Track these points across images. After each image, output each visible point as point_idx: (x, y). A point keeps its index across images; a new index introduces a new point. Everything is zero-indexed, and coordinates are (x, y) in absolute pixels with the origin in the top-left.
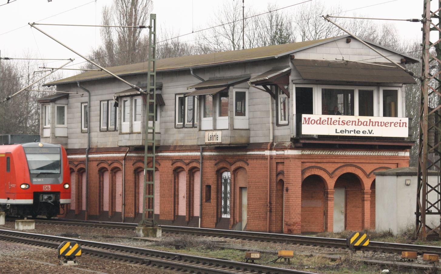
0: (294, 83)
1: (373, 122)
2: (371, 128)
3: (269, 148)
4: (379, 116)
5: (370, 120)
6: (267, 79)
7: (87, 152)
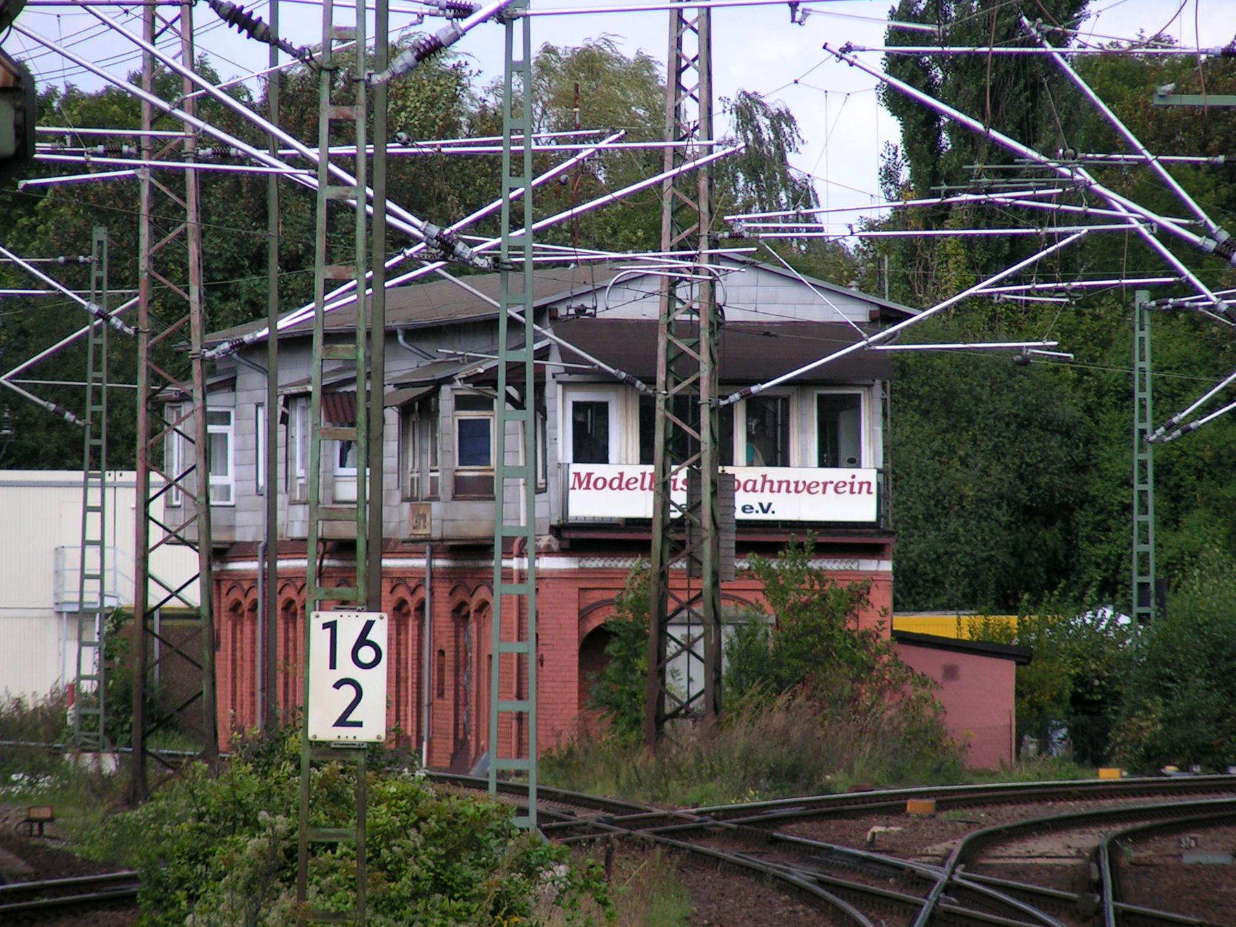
0: (558, 382)
1: (772, 482)
2: (766, 498)
3: (515, 551)
4: (804, 465)
5: (764, 477)
6: (480, 374)
7: (260, 553)
